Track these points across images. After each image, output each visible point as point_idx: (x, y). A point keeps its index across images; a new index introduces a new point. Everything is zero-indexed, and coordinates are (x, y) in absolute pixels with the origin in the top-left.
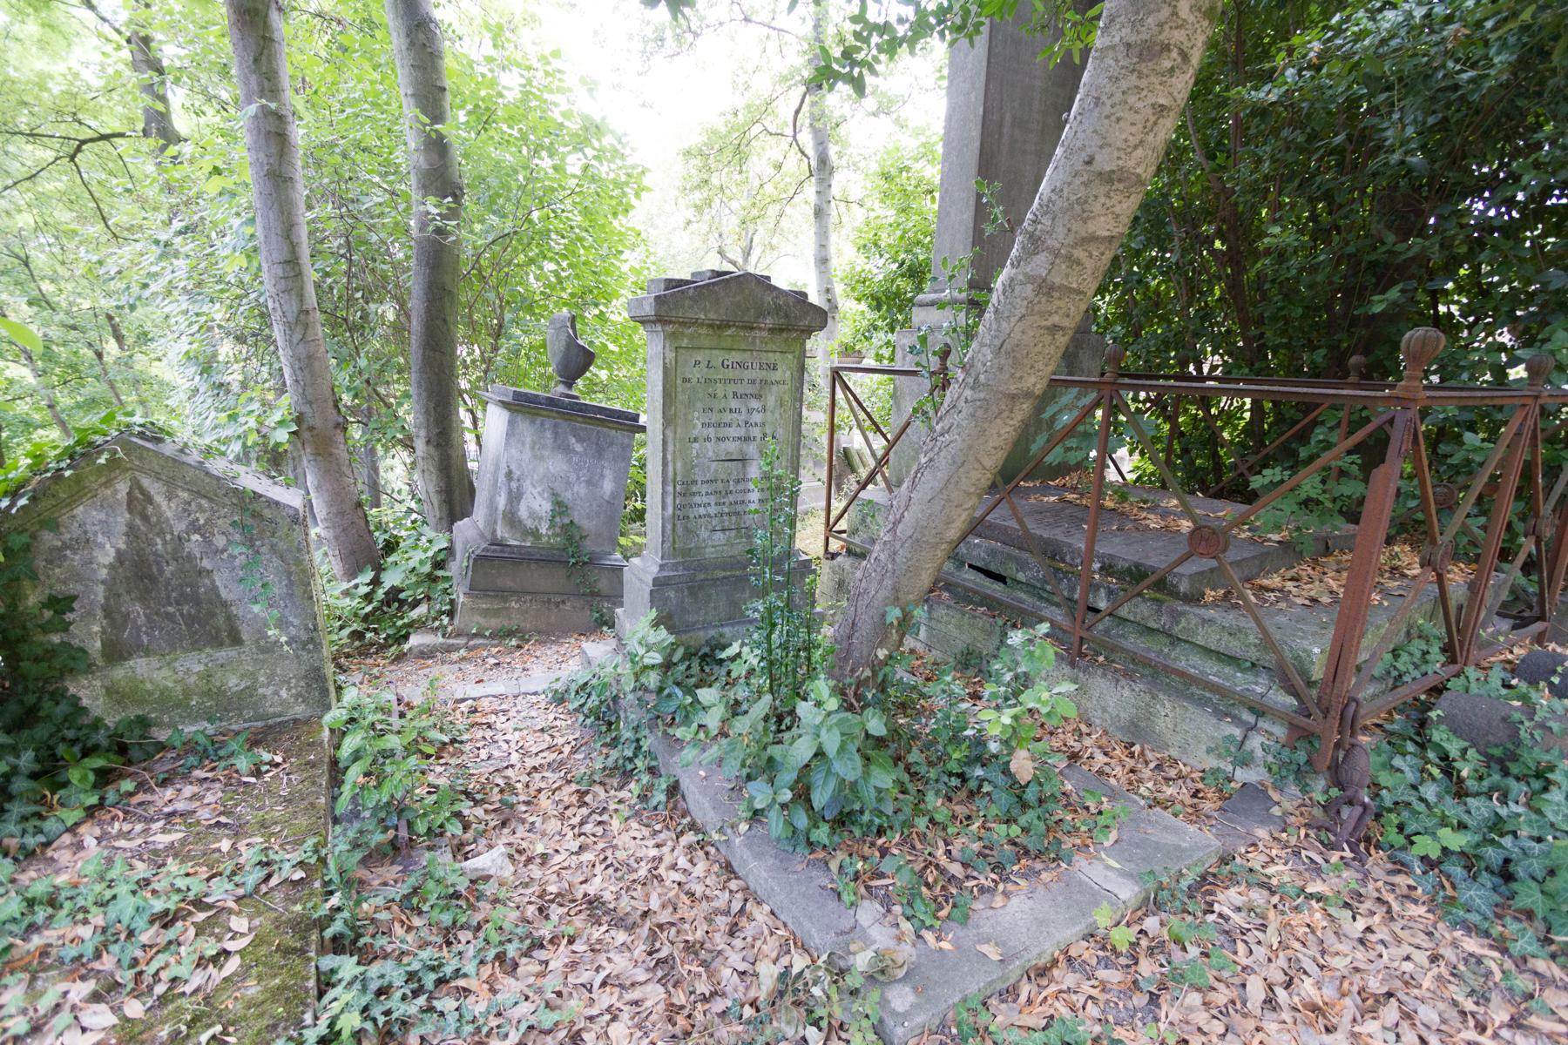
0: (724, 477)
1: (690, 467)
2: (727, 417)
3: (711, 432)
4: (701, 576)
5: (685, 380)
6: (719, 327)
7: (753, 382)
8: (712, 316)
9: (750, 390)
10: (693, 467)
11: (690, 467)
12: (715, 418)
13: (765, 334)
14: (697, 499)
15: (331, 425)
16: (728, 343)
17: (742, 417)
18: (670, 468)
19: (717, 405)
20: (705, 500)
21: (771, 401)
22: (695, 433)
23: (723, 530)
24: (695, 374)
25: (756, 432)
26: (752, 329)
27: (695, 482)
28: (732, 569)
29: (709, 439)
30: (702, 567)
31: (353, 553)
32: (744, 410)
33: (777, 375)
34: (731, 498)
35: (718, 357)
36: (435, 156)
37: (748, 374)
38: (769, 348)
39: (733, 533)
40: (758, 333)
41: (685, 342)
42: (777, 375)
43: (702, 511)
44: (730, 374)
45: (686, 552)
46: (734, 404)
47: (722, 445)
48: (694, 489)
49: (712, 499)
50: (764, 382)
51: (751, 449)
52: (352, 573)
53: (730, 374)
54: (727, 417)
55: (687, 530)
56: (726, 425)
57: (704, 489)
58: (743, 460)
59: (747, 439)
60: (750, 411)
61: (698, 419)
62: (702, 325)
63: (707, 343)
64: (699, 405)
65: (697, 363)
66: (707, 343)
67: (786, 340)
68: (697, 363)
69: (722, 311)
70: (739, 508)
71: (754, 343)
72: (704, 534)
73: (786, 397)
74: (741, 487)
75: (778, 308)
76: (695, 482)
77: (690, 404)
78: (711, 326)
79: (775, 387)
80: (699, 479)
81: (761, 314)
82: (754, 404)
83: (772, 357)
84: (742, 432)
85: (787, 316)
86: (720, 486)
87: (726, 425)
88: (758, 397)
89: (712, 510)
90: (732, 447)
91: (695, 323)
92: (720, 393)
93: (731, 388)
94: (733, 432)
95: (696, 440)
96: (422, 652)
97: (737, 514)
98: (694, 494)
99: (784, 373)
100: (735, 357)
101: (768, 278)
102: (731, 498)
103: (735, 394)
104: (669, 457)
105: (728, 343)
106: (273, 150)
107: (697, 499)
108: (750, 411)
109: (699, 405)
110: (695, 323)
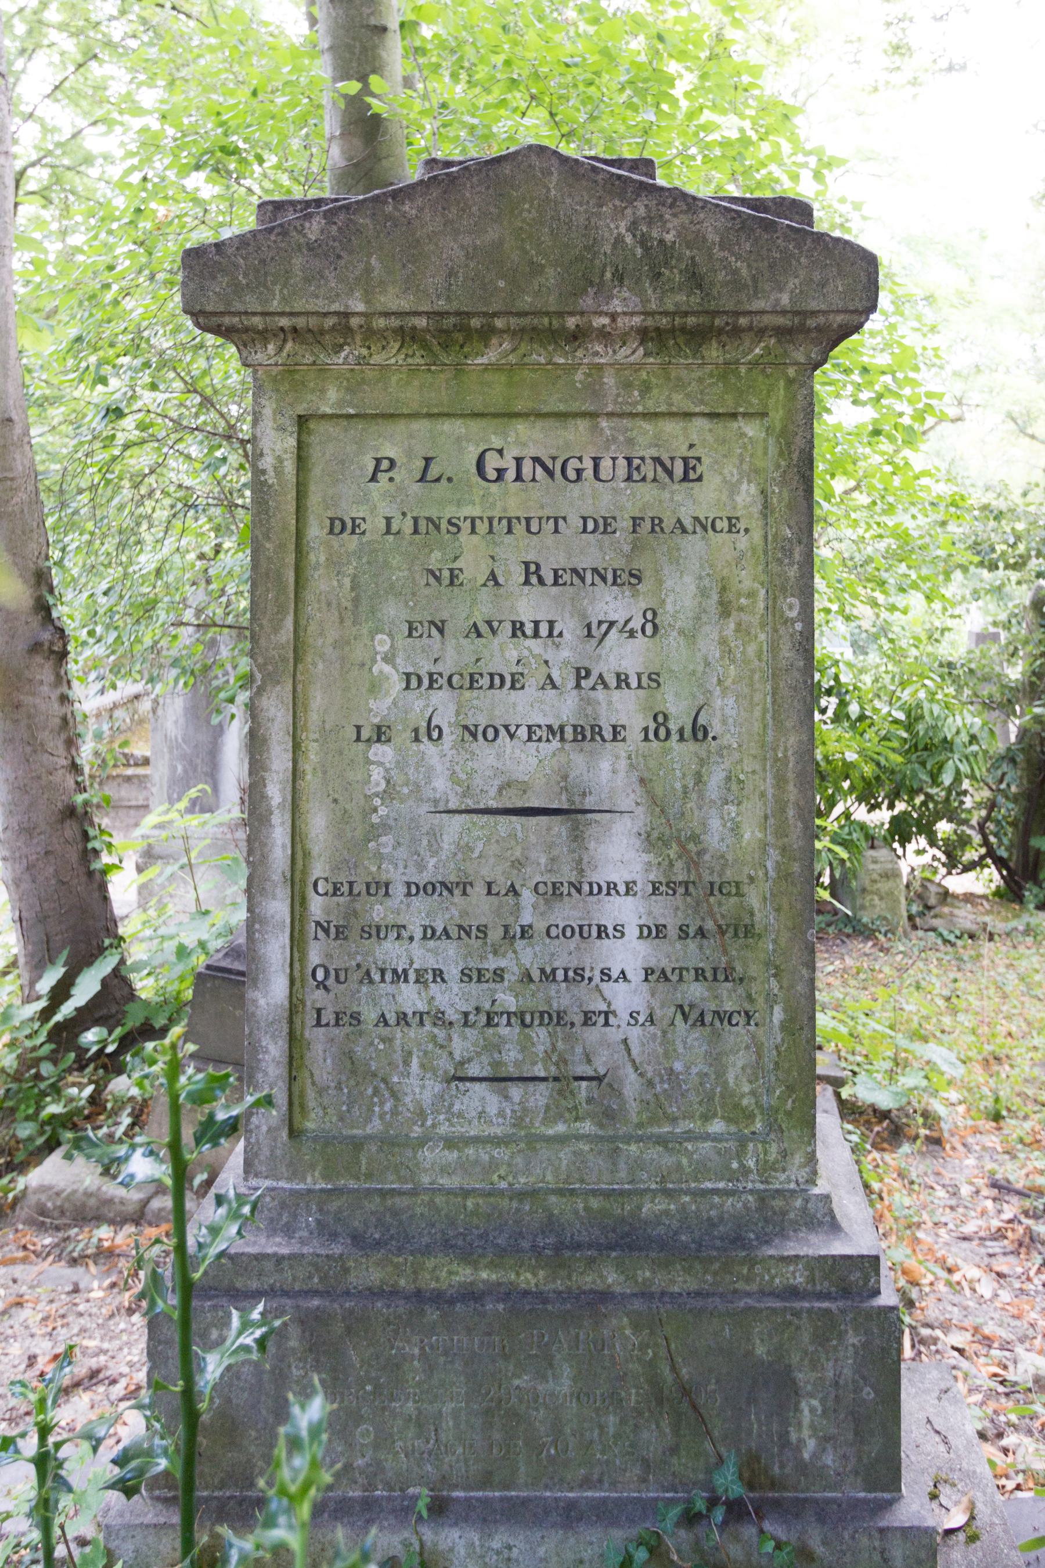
0: (497, 872)
1: (360, 831)
2: (503, 654)
3: (442, 705)
4: (370, 1273)
5: (338, 526)
6: (447, 336)
7: (605, 526)
8: (393, 299)
9: (591, 553)
10: (374, 832)
11: (360, 831)
12: (454, 655)
13: (631, 353)
14: (391, 952)
15: (21, 646)
16: (496, 392)
17: (564, 656)
18: (279, 835)
19: (460, 611)
20: (422, 956)
21: (681, 593)
22: (380, 708)
23: (497, 1079)
24: (376, 505)
25: (625, 708)
26: (578, 337)
27: (381, 888)
28: (502, 1255)
29: (432, 732)
30: (385, 1234)
31: (42, 919)
32: (569, 627)
33: (705, 499)
34: (528, 956)
35: (459, 443)
36: (357, 142)
37: (579, 500)
38: (657, 401)
39: (540, 1096)
40: (601, 353)
41: (330, 400)
42: (705, 499)
43: (410, 997)
44: (512, 500)
45: (342, 1151)
46: (529, 605)
47: (486, 757)
48: (378, 912)
49: (450, 957)
50: (649, 527)
51: (608, 773)
52: (38, 966)
53: (512, 500)
54: (503, 654)
55: (350, 1064)
56: (496, 681)
57: (417, 914)
58: (573, 813)
59: (586, 734)
60: (594, 632)
61: (387, 661)
62: (381, 335)
63: (412, 395)
64: (393, 611)
65: (383, 466)
66: (412, 396)
67: (728, 369)
68: (383, 466)
69: (433, 281)
70: (561, 997)
71: (594, 390)
72: (419, 1088)
73: (746, 578)
74: (566, 913)
75: (656, 259)
76: (381, 888)
77: (359, 607)
78: (408, 336)
79: (693, 546)
80: (397, 876)
81: (586, 276)
82: (611, 604)
83: (675, 438)
84: (565, 708)
85: (695, 279)
86: (480, 907)
87: (496, 681)
88: (629, 578)
89: (452, 997)
90: (527, 763)
91: (343, 329)
92: (473, 566)
93: (515, 551)
94: (527, 706)
95: (381, 734)
96: (43, 1211)
97: (557, 1019)
98: (376, 932)
99: (730, 485)
100: (527, 439)
101: (646, 166)
102: (528, 956)
103: (532, 573)
104: (276, 792)
105: (496, 392)
106: (801, 337)
107: (391, 952)
108: (594, 632)
109: (393, 611)
110: (343, 329)
